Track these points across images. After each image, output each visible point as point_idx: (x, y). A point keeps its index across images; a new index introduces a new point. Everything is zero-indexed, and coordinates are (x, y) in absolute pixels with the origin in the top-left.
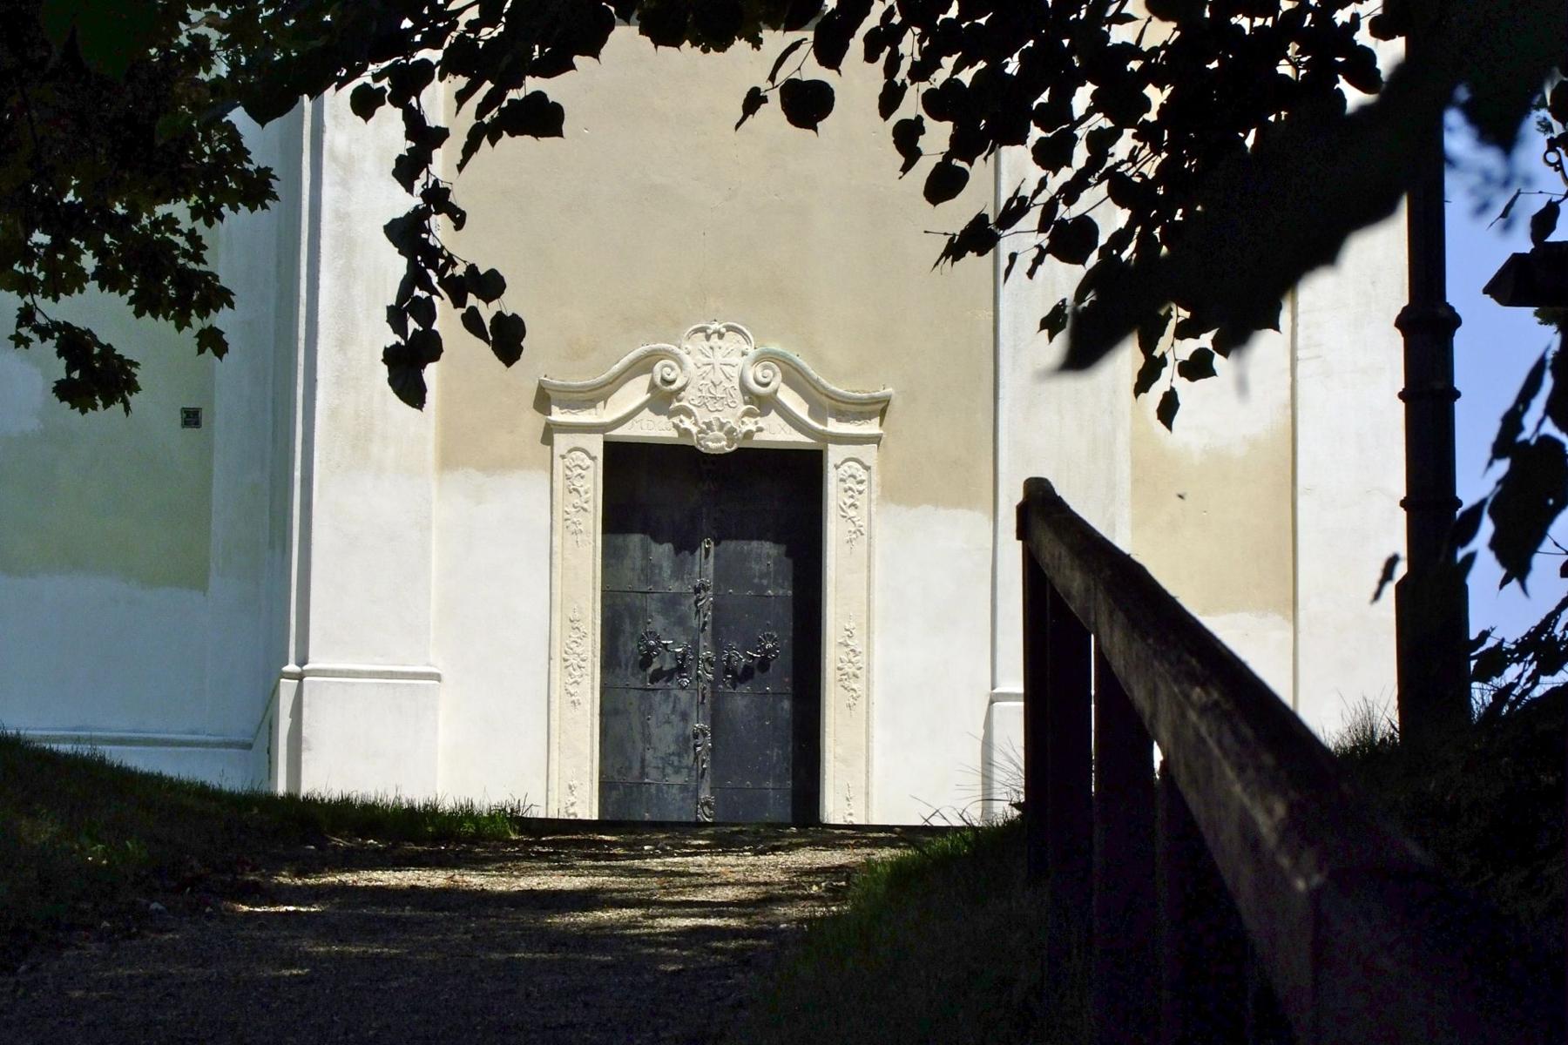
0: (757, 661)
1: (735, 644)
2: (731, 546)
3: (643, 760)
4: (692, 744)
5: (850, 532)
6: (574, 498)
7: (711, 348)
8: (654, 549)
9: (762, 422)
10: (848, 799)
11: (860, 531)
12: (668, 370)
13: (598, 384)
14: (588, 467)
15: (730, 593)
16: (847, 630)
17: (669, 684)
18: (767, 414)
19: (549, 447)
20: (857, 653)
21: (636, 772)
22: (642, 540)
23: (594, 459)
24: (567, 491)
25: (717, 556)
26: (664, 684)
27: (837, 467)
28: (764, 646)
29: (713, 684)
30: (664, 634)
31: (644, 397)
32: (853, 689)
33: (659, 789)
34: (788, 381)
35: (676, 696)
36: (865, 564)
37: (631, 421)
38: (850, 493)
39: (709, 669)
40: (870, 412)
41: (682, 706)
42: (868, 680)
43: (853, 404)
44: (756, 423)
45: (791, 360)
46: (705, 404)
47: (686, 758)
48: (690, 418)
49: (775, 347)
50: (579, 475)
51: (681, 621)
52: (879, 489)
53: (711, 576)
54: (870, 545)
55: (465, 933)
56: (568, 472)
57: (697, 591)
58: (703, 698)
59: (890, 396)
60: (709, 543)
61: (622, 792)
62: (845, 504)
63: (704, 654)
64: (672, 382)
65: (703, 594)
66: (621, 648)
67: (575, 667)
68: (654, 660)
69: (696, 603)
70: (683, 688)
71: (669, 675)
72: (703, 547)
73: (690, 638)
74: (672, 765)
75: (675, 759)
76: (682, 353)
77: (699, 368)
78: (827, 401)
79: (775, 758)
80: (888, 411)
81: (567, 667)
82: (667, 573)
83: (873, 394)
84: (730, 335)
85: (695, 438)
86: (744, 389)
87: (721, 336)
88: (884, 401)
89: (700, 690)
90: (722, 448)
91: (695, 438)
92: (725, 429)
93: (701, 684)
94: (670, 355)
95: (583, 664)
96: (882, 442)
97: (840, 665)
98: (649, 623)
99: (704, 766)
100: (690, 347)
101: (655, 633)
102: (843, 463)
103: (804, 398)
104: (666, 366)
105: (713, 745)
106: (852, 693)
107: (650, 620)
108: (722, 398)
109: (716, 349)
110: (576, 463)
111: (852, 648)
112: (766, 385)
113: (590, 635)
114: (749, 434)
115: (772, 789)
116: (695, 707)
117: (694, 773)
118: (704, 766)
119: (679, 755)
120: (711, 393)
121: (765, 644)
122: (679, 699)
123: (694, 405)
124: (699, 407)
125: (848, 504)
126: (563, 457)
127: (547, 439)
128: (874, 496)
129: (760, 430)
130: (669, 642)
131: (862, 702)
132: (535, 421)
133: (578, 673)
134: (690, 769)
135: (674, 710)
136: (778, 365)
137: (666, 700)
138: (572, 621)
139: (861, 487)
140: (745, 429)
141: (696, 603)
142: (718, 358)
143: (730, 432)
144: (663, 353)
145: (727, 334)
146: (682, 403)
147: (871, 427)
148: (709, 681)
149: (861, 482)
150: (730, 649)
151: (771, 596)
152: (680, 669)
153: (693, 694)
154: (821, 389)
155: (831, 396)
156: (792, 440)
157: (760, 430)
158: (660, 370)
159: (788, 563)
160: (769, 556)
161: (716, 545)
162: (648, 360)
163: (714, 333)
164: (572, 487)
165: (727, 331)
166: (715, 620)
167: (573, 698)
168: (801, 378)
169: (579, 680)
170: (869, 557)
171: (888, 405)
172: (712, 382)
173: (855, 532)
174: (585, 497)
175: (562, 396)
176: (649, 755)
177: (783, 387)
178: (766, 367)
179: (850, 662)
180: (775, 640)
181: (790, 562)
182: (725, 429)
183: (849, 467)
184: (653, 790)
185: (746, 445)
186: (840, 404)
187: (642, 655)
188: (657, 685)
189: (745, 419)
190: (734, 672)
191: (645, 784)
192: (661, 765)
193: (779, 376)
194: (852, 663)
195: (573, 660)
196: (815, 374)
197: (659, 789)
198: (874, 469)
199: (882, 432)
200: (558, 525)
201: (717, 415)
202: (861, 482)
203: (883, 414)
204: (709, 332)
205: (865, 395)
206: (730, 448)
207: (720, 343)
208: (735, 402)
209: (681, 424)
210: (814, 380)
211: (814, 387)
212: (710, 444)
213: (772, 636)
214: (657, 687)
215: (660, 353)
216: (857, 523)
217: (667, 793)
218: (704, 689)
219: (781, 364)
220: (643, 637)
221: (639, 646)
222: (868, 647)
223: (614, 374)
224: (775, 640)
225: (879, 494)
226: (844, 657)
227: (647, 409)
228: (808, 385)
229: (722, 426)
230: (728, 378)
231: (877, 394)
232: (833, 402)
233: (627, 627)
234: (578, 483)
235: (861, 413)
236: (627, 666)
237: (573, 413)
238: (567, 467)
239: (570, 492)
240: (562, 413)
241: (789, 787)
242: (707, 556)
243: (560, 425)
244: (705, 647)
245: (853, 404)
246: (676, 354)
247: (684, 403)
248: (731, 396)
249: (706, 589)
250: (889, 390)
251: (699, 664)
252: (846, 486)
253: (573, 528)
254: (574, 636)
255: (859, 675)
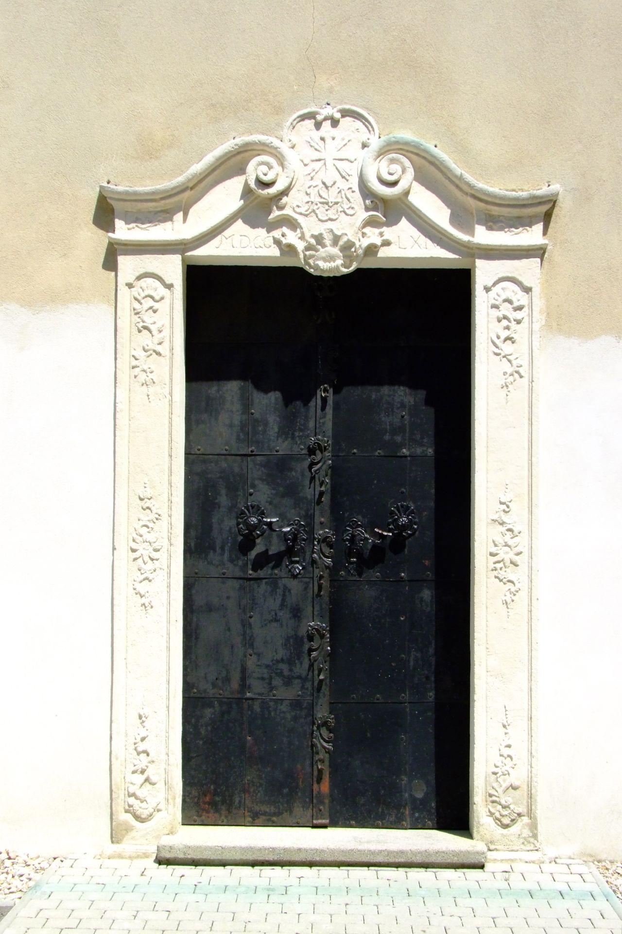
0: (388, 541)
1: (360, 517)
2: (355, 393)
3: (244, 670)
4: (306, 647)
5: (505, 374)
6: (145, 339)
7: (322, 139)
8: (256, 401)
9: (389, 233)
10: (504, 726)
11: (517, 372)
12: (264, 168)
13: (172, 189)
14: (162, 298)
15: (354, 454)
16: (501, 503)
17: (276, 572)
18: (395, 222)
19: (113, 274)
20: (516, 532)
21: (235, 685)
22: (242, 389)
23: (169, 287)
24: (135, 331)
25: (337, 407)
26: (270, 572)
27: (487, 289)
28: (396, 520)
29: (333, 571)
30: (269, 507)
31: (236, 203)
32: (509, 581)
33: (264, 705)
34: (421, 177)
35: (285, 587)
36: (526, 416)
37: (219, 237)
38: (505, 323)
39: (327, 550)
40: (530, 217)
41: (292, 599)
42: (531, 568)
43: (509, 206)
44: (381, 234)
45: (426, 151)
46: (314, 211)
47: (298, 665)
48: (295, 231)
49: (406, 135)
50: (151, 308)
51: (292, 491)
52: (544, 317)
53: (330, 433)
54: (531, 390)
55: (265, 621)
56: (136, 305)
57: (311, 452)
58: (320, 587)
59: (557, 194)
60: (325, 390)
61: (217, 709)
62: (498, 337)
63: (320, 533)
64: (268, 185)
65: (319, 456)
66: (215, 526)
67: (147, 559)
68: (258, 541)
69: (310, 467)
70: (295, 577)
71: (277, 560)
72: (319, 397)
73: (303, 512)
74: (280, 674)
75: (284, 667)
76: (284, 148)
77: (306, 165)
78: (472, 202)
79: (412, 663)
80: (553, 217)
81: (135, 559)
82: (274, 428)
83: (535, 192)
84: (347, 123)
85: (302, 256)
86: (366, 191)
87: (335, 123)
88: (550, 201)
89: (316, 579)
90: (337, 268)
91: (302, 256)
92: (341, 243)
93: (316, 571)
94: (268, 150)
95: (155, 555)
96: (546, 256)
97: (494, 550)
98: (251, 494)
99: (322, 677)
100: (295, 140)
101: (259, 508)
102: (495, 284)
103: (443, 202)
104: (263, 163)
105: (331, 650)
106: (509, 585)
107: (252, 491)
108: (337, 203)
109: (329, 141)
110: (146, 293)
111: (509, 526)
112: (394, 184)
113: (165, 517)
114: (371, 250)
115: (409, 703)
116: (310, 599)
117: (308, 685)
118: (322, 677)
119: (290, 662)
120: (321, 197)
121: (399, 518)
122: (290, 591)
123: (301, 214)
124: (306, 216)
125: (503, 338)
126: (130, 286)
127: (110, 263)
128: (536, 327)
129: (386, 243)
130: (274, 520)
131: (523, 595)
132: (98, 241)
133: (150, 565)
134: (304, 680)
135: (282, 605)
136: (404, 155)
137: (273, 592)
138: (141, 499)
139: (518, 315)
140: (365, 243)
141: (310, 467)
142: (330, 151)
143: (348, 247)
144: (262, 148)
145: (341, 120)
146: (284, 212)
147: (532, 236)
148: (327, 567)
149: (520, 308)
150: (355, 526)
151: (406, 457)
152: (290, 552)
153: (307, 583)
154: (465, 188)
155: (478, 196)
156: (428, 256)
157: (386, 243)
158: (255, 169)
159: (429, 413)
160: (403, 406)
161: (335, 393)
162: (239, 157)
163: (325, 119)
164: (141, 324)
165: (343, 116)
166: (334, 488)
167: (143, 600)
168: (439, 175)
169: (151, 577)
170: (531, 406)
171: (554, 206)
172: (324, 183)
173: (512, 375)
174: (158, 337)
175: (128, 206)
176: (251, 663)
177: (415, 185)
178: (392, 161)
179: (506, 545)
180: (412, 512)
181: (431, 411)
182: (341, 243)
183: (503, 289)
184: (257, 707)
185: (370, 264)
186: (489, 207)
187: (242, 535)
188: (261, 573)
189: (368, 230)
190: (359, 555)
191: (247, 699)
192: (266, 676)
193: (410, 173)
194: (509, 547)
195: (144, 550)
196: (458, 170)
197: (264, 705)
198: (536, 291)
199: (546, 242)
200: (124, 376)
201: (329, 225)
202: (520, 308)
203: (547, 218)
204: (319, 118)
205: (524, 194)
206: (348, 268)
207: (334, 132)
208: (353, 208)
209: (283, 239)
210: (456, 176)
211: (457, 186)
212: (321, 264)
213: (408, 508)
214: (262, 576)
215: (255, 147)
216: (514, 362)
217: (275, 710)
218: (321, 577)
219: (414, 157)
220: (243, 513)
221: (238, 524)
222: (530, 525)
223: (195, 176)
224: (412, 512)
225: (543, 322)
226: (500, 540)
227: (240, 222)
228: (447, 182)
229: (336, 239)
230: (343, 177)
231: (538, 193)
232: (482, 205)
233: (224, 500)
234: (148, 318)
235: (519, 218)
236: (222, 548)
237: (141, 228)
238: (136, 299)
239: (140, 331)
240: (129, 229)
241: (431, 699)
242: (323, 408)
243: (125, 245)
244: (321, 523)
245: (509, 206)
246: (276, 148)
247: (287, 211)
248: (348, 200)
249: (322, 449)
250: (555, 187)
251: (314, 545)
252: (500, 315)
253: (142, 377)
254: (146, 517)
255: (519, 563)
